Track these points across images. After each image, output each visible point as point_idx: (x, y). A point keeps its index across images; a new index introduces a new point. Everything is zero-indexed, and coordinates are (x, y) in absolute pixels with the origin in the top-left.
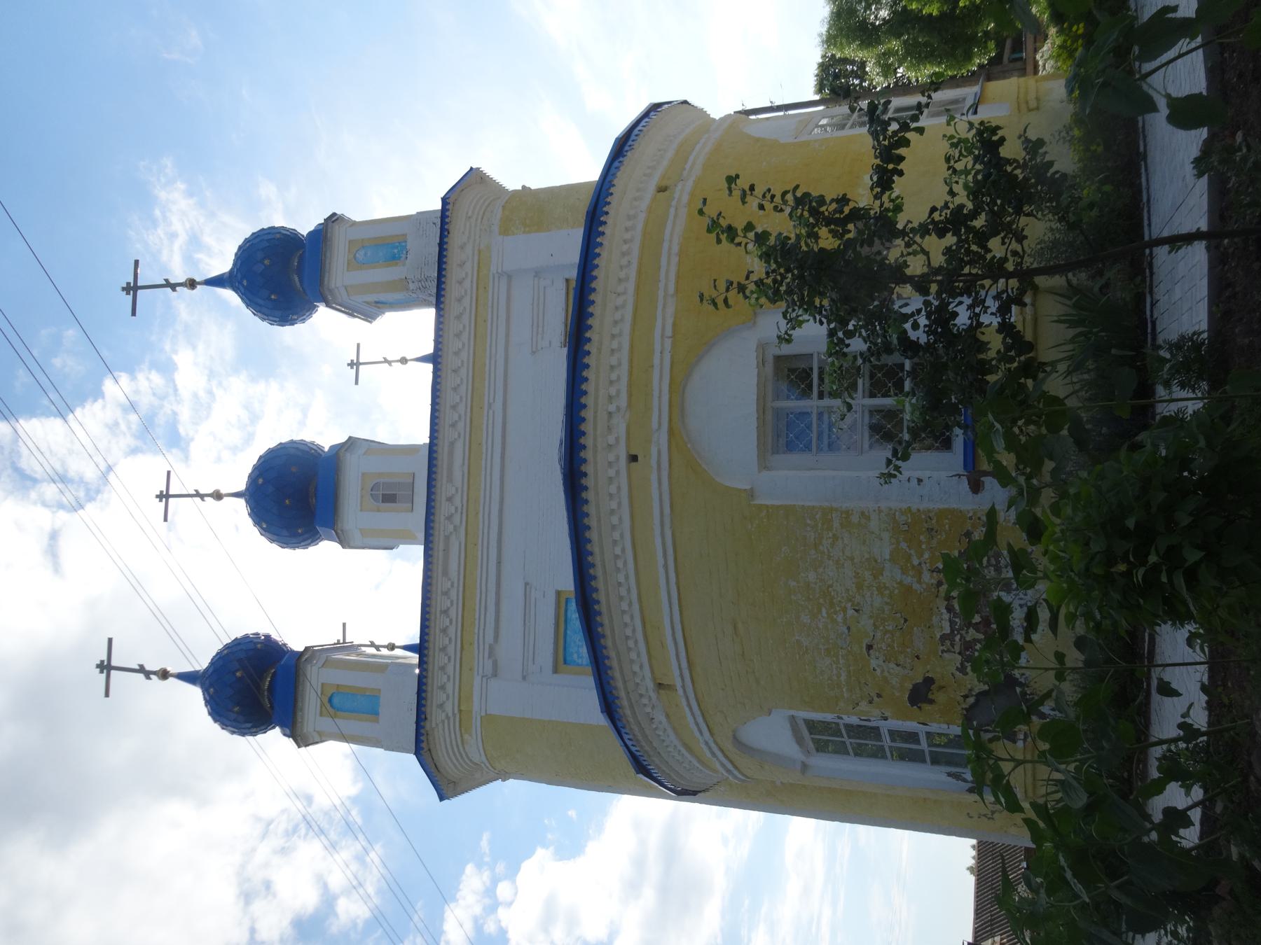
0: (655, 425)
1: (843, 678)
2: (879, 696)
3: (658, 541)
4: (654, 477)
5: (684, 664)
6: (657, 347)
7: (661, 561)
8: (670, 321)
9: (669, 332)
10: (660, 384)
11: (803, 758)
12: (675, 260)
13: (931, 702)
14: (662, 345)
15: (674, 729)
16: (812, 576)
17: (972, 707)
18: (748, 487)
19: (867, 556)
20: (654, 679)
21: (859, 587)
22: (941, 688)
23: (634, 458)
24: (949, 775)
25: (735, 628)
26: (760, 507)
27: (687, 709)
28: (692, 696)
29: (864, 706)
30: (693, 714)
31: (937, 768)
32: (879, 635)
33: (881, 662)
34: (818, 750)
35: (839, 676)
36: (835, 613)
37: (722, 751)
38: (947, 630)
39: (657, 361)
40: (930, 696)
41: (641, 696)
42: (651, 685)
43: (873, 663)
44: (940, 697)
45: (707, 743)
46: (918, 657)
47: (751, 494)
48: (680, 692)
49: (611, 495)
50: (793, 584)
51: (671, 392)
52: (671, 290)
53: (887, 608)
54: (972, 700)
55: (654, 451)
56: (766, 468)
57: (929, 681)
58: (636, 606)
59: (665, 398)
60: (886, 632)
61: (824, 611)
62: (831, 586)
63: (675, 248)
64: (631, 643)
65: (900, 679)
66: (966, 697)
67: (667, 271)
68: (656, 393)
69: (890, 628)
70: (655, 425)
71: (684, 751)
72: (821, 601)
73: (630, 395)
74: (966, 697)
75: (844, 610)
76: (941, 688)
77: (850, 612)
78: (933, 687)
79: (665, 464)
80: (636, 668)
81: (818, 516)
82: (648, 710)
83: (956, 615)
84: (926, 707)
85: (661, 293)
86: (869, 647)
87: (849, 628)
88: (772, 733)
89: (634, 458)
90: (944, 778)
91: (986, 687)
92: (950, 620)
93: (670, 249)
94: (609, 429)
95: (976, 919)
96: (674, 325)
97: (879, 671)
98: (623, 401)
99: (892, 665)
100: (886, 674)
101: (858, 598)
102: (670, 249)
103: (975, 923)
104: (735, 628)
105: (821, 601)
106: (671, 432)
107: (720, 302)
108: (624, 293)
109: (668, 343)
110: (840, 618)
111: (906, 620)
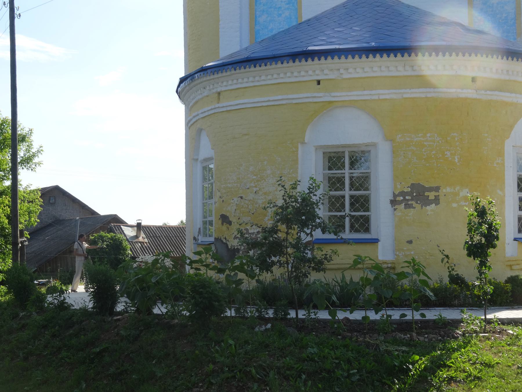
0: (333, 94)
1: (229, 185)
2: (223, 201)
3: (280, 97)
4: (309, 95)
5: (229, 108)
6: (373, 92)
7: (271, 98)
8: (387, 97)
9: (382, 97)
10: (355, 95)
11: (199, 160)
12: (423, 96)
13: (222, 224)
14: (374, 95)
15: (202, 98)
16: (269, 172)
17: (222, 241)
18: (306, 141)
19: (278, 197)
20: (222, 91)
21: (265, 193)
22: (228, 228)
23: (319, 82)
24: (200, 229)
25: (246, 135)
26: (297, 148)
27: (210, 108)
28: (216, 111)
29: (218, 194)
30: (208, 111)
31: (202, 223)
32: (247, 202)
33: (236, 202)
34: (203, 167)
35: (229, 183)
36: (255, 183)
37: (196, 121)
38: (250, 231)
39: (366, 92)
40: (225, 223)
41: (213, 85)
42: (219, 90)
43: (236, 199)
44: (224, 227)
45: (198, 115)
46: (239, 219)
47: (303, 143)
48: (217, 106)
49: (300, 72)
50: (265, 163)
51: (350, 101)
52: (405, 96)
53: (258, 205)
54: (224, 241)
55: (321, 94)
56: (316, 149)
57: (230, 223)
58: (252, 84)
59: (347, 98)
60: (248, 205)
61: (255, 177)
62: (265, 180)
63: (429, 95)
64: (235, 81)
65: (230, 211)
66: (225, 239)
67: (416, 93)
68: (349, 94)
69: (250, 207)
70: (333, 94)
71: (194, 101)
72: (259, 176)
73: (350, 79)
74: (225, 239)
75: (256, 187)
76: (228, 228)
77: (255, 189)
78: (228, 225)
79: (315, 100)
80: (225, 84)
81: (293, 175)
82: (208, 88)
83: (256, 235)
84: (220, 222)
85: (402, 91)
86: (242, 198)
87: (248, 188)
88: (206, 150)
89: (319, 82)
90: (198, 227)
91: (230, 247)
92: (254, 233)
93: (430, 92)
94: (332, 70)
95: (156, 227)
96: (386, 99)
97: (232, 201)
98: (346, 76)
99: (235, 207)
100: (232, 205)
101: (261, 193)
102: (430, 92)
103: (153, 226)
104: (246, 135)
105: (259, 176)
106: (330, 102)
107: (279, 183)
108: (405, 70)
109: (376, 97)
110: (253, 185)
111: (253, 214)
